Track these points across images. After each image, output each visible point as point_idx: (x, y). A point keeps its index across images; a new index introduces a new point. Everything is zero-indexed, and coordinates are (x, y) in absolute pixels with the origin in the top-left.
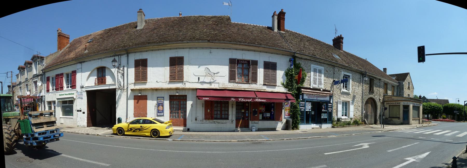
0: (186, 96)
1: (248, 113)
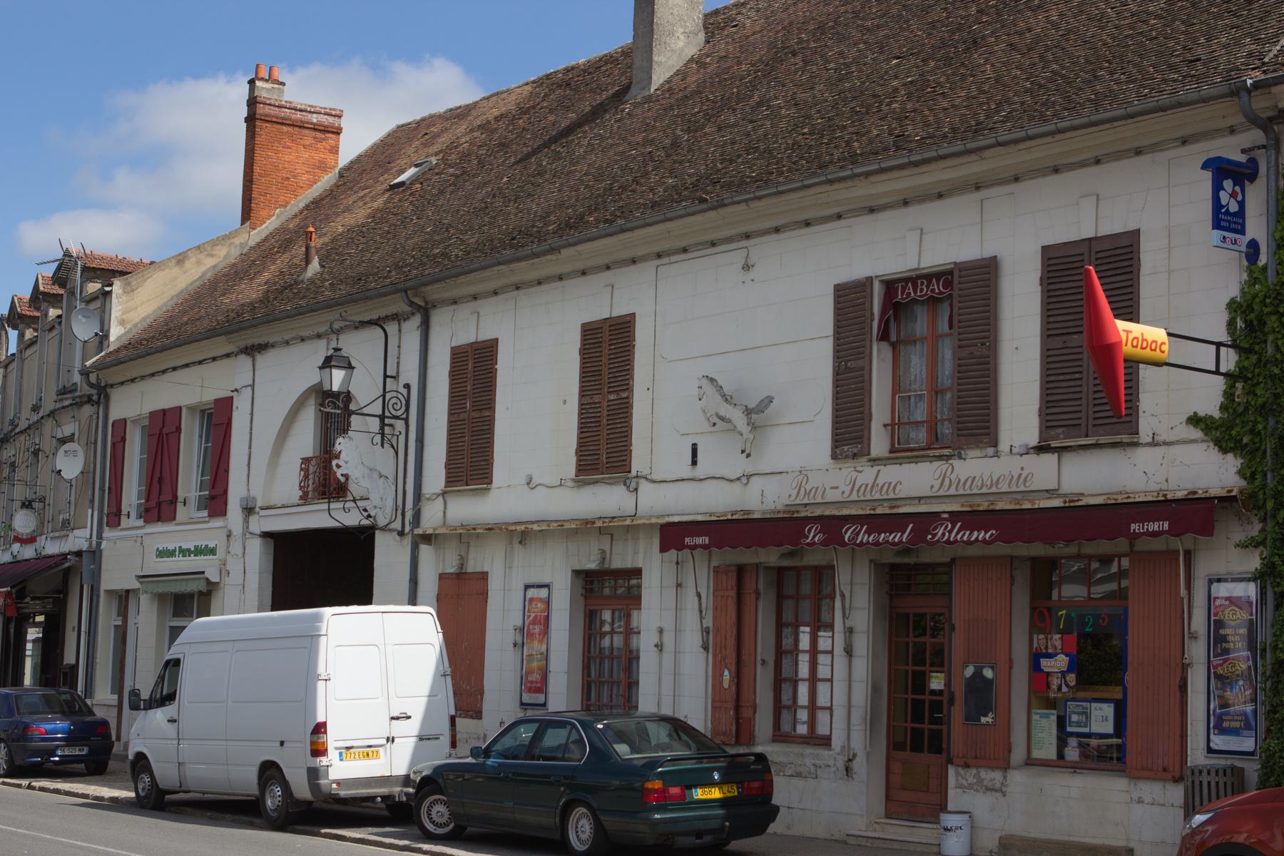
0: (637, 572)
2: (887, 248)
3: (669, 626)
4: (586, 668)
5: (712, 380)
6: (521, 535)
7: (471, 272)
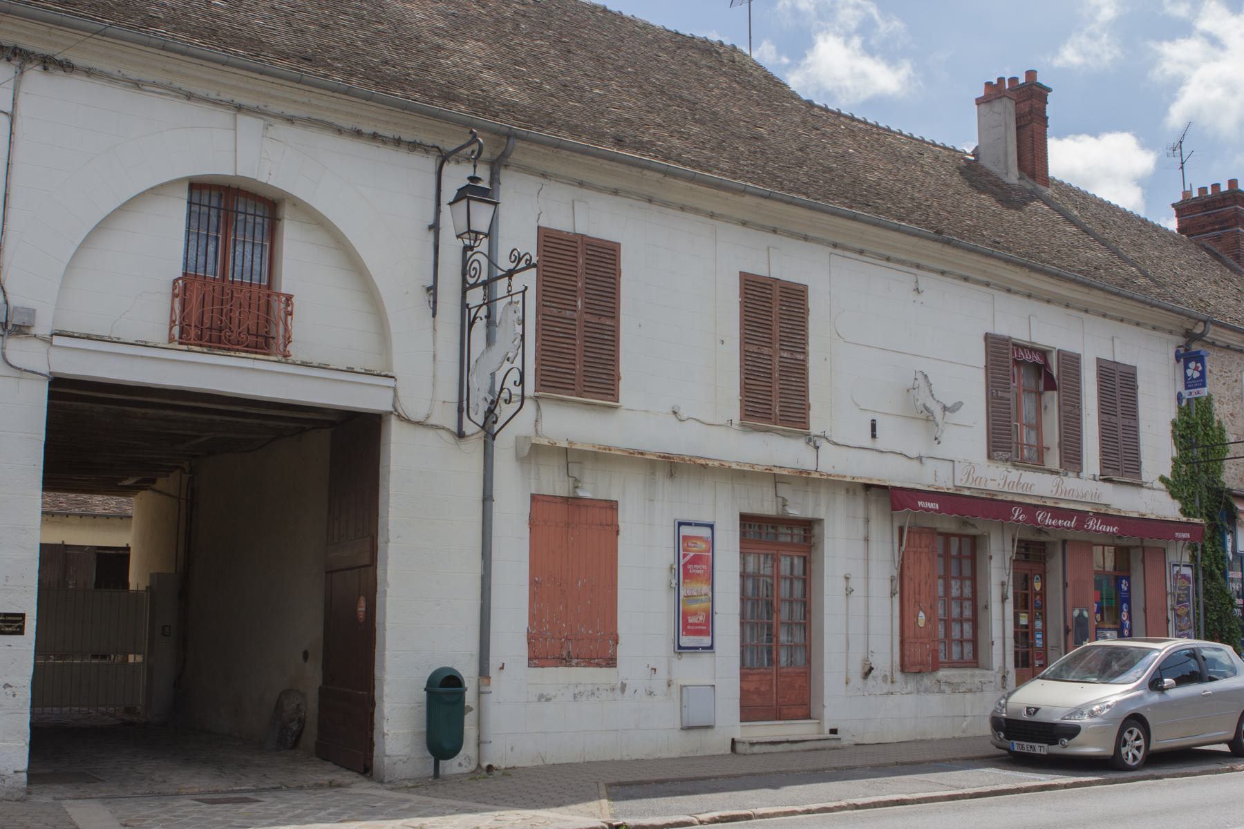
0: (612, 506)
1: (1044, 631)
2: (1050, 330)
4: (807, 612)
5: (926, 376)
7: (957, 246)
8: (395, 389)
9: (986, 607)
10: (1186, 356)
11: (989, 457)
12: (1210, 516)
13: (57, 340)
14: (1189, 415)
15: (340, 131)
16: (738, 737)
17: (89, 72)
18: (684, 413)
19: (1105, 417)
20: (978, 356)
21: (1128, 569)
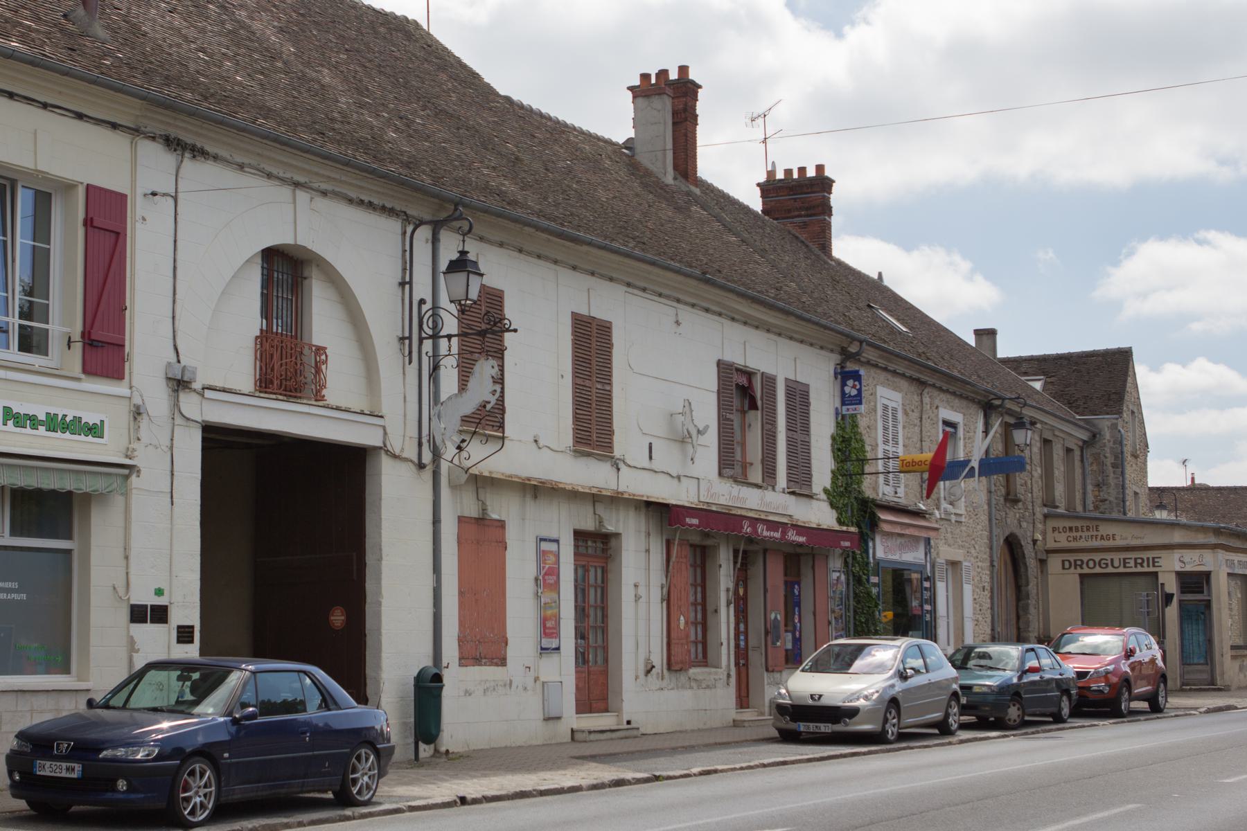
3: (642, 583)
4: (605, 616)
6: (536, 490)
8: (384, 428)
9: (716, 611)
10: (844, 376)
11: (720, 474)
12: (859, 526)
13: (208, 394)
14: (843, 429)
15: (350, 201)
16: (575, 727)
17: (216, 158)
18: (541, 443)
19: (579, 381)
20: (712, 382)
21: (799, 574)
